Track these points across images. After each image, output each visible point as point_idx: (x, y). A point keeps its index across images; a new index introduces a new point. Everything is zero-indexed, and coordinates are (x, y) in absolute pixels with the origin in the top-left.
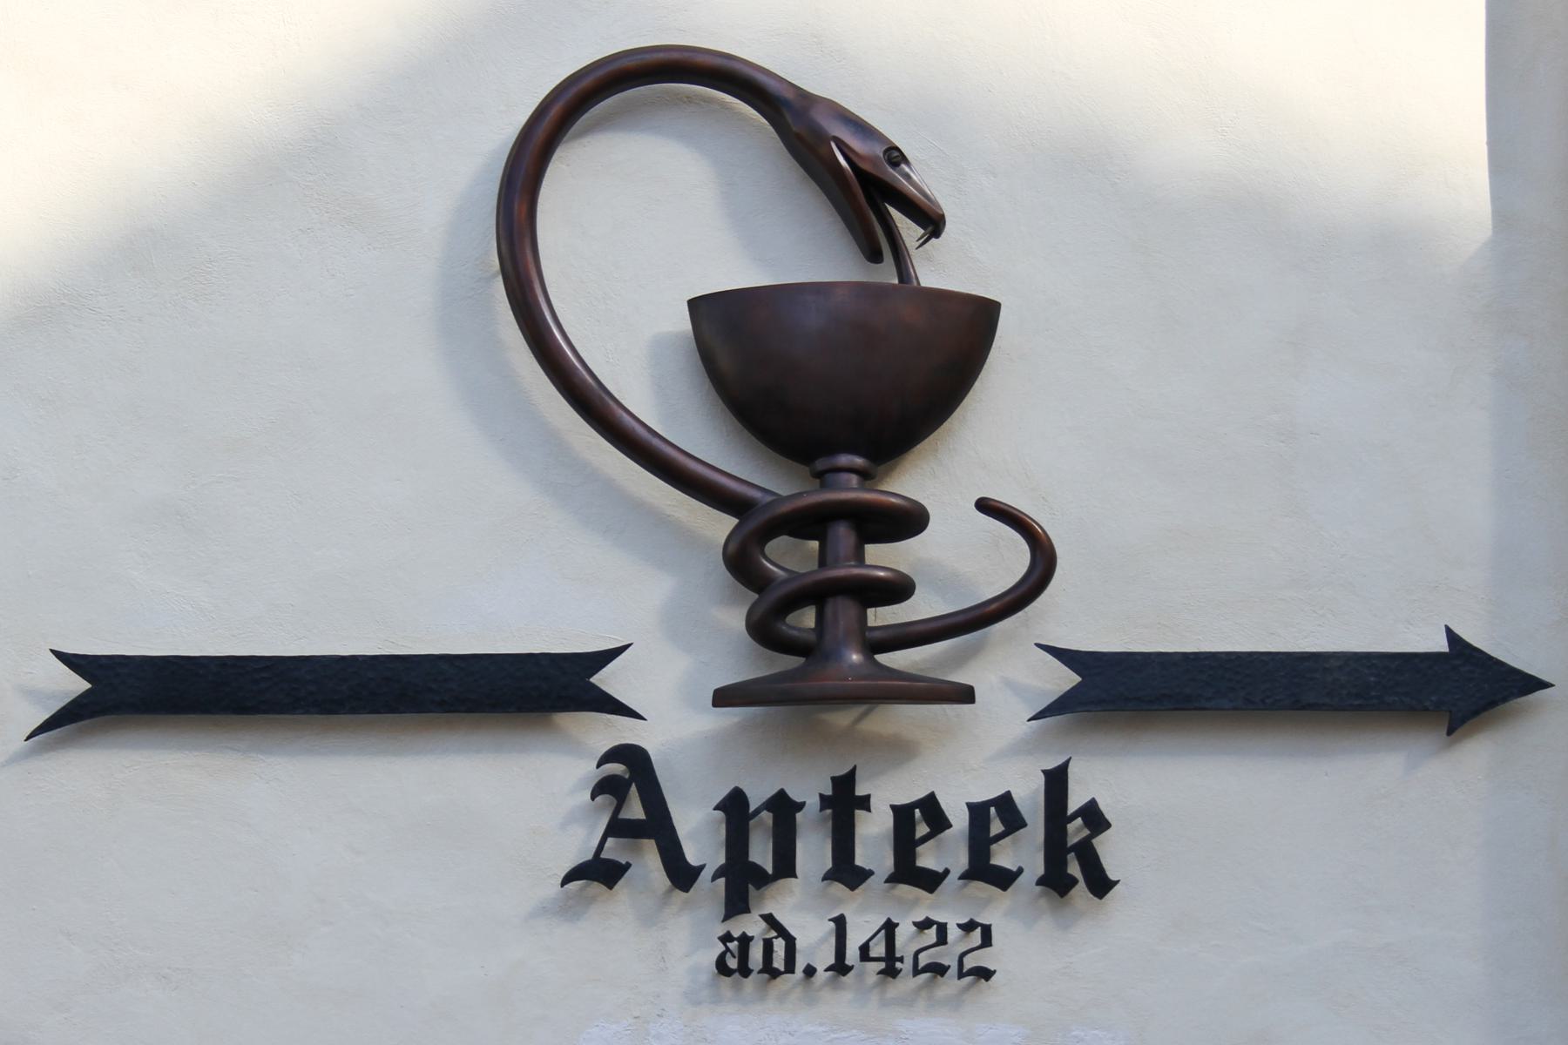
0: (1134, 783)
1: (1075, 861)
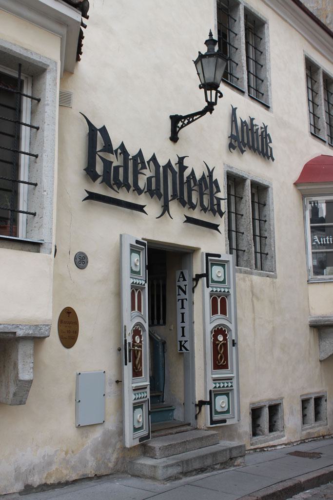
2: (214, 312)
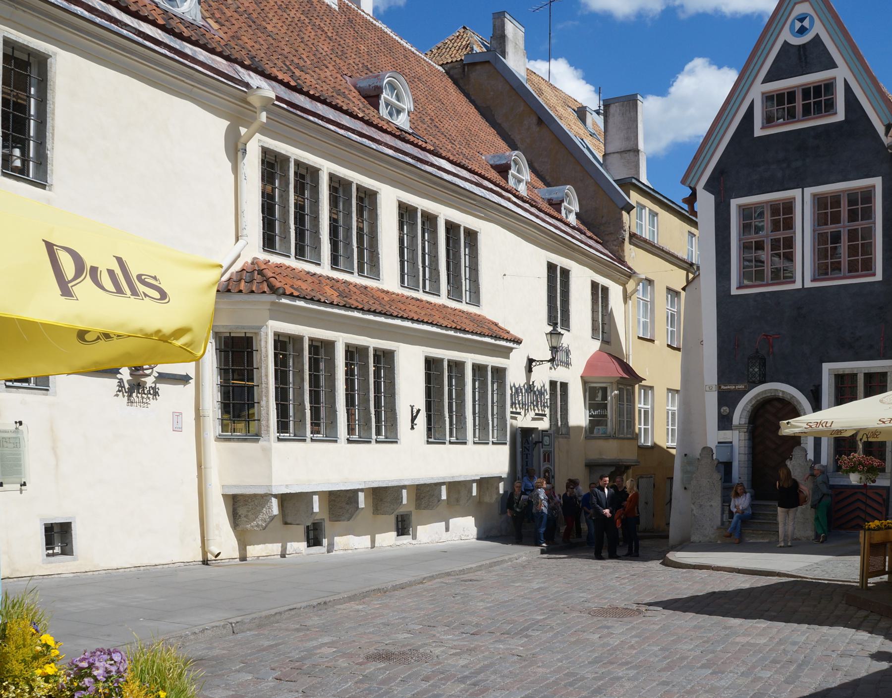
0: (162, 387)
1: (156, 394)
2: (545, 461)
